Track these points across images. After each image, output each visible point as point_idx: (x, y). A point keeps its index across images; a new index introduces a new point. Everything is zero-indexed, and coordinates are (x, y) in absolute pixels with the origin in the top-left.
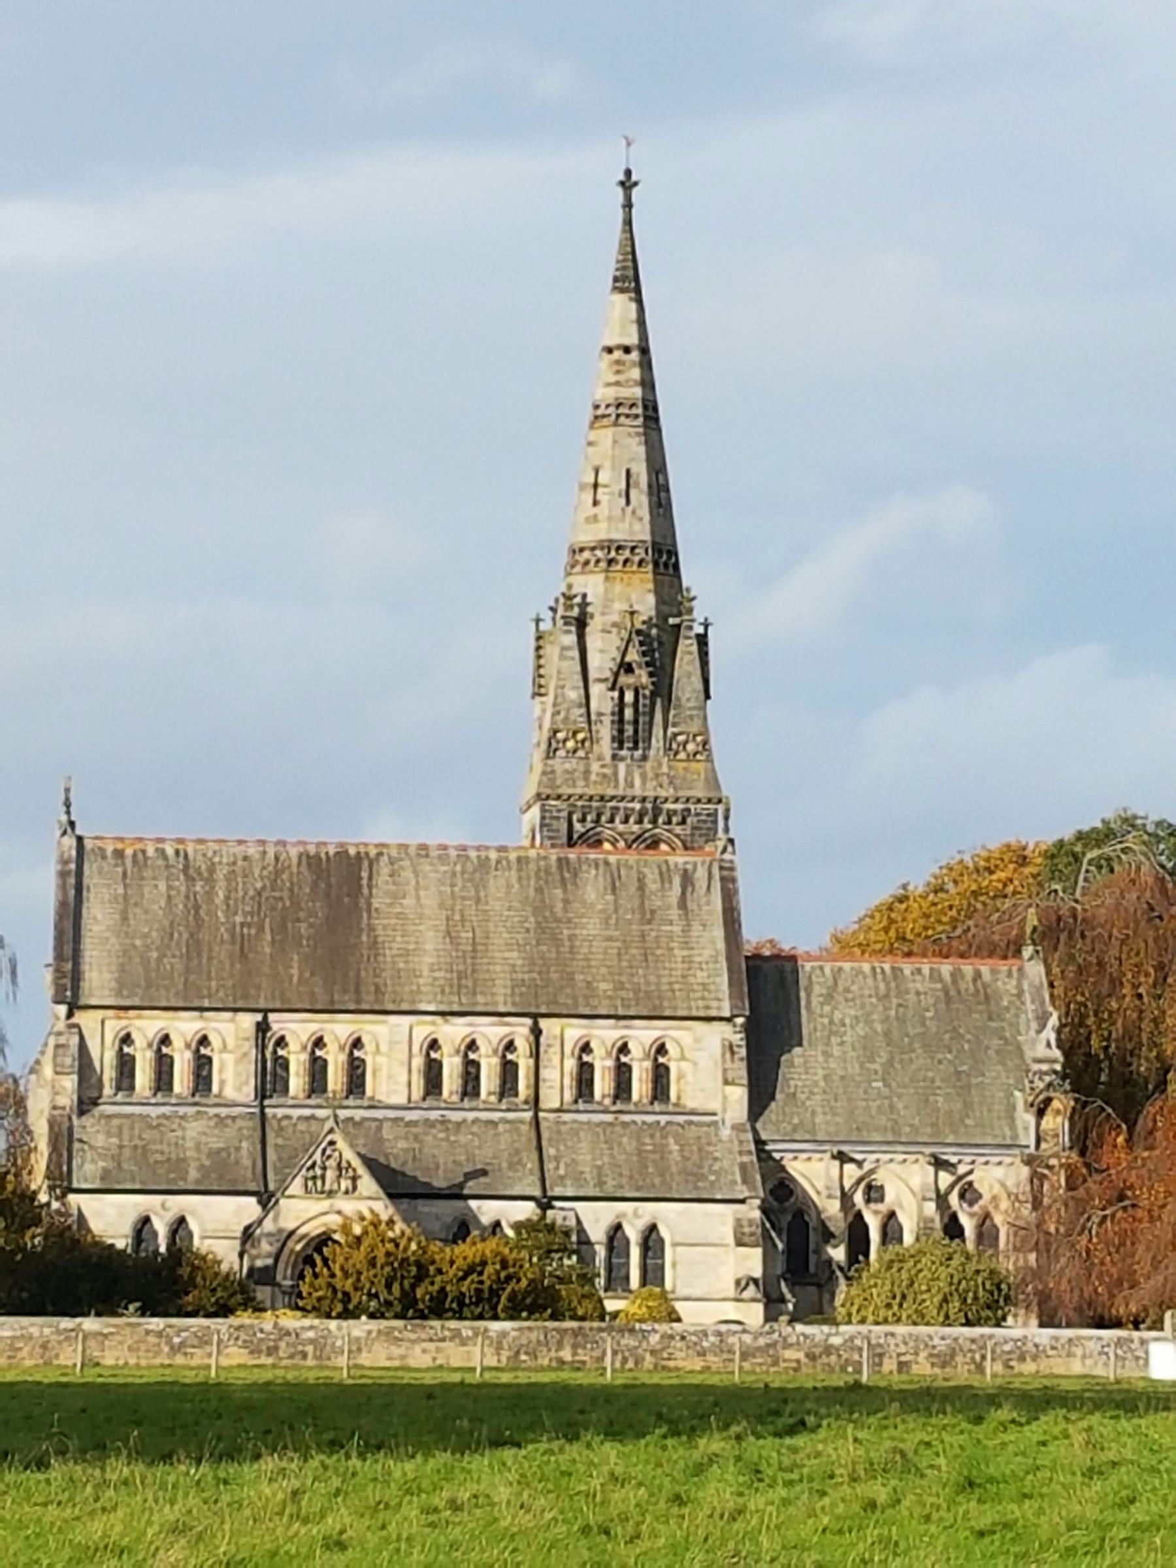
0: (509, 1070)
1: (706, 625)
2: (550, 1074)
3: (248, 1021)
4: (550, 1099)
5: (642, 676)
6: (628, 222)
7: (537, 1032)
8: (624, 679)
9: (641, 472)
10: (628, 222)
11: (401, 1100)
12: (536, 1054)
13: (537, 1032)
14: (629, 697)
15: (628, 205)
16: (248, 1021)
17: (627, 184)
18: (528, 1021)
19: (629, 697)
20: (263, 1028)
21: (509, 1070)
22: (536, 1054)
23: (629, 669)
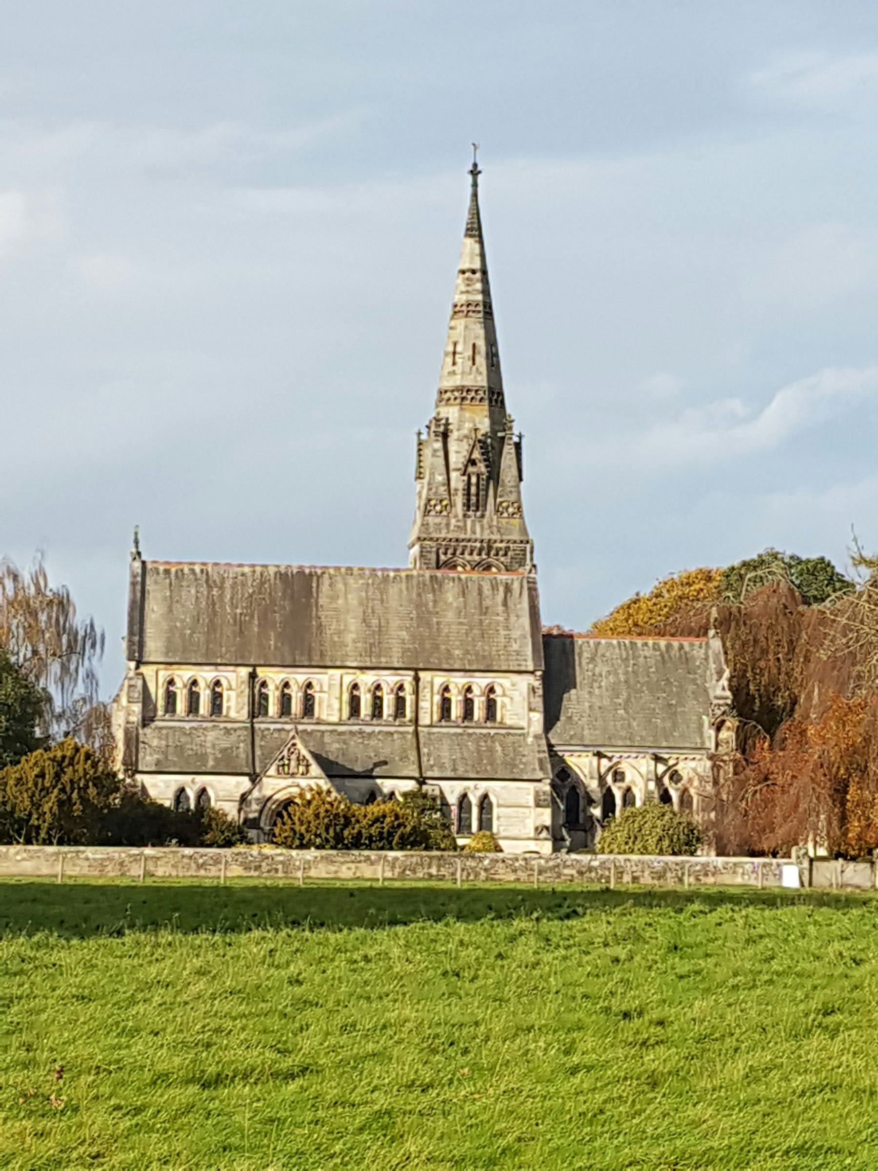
0: (400, 702)
1: (520, 437)
2: (424, 704)
3: (244, 672)
4: (425, 719)
5: (482, 467)
6: (475, 195)
7: (417, 679)
8: (471, 469)
9: (481, 344)
10: (475, 195)
11: (335, 719)
12: (416, 692)
13: (417, 679)
14: (474, 480)
15: (475, 185)
16: (244, 672)
17: (475, 172)
18: (412, 673)
19: (474, 480)
20: (253, 676)
21: (400, 702)
22: (416, 692)
23: (473, 462)
